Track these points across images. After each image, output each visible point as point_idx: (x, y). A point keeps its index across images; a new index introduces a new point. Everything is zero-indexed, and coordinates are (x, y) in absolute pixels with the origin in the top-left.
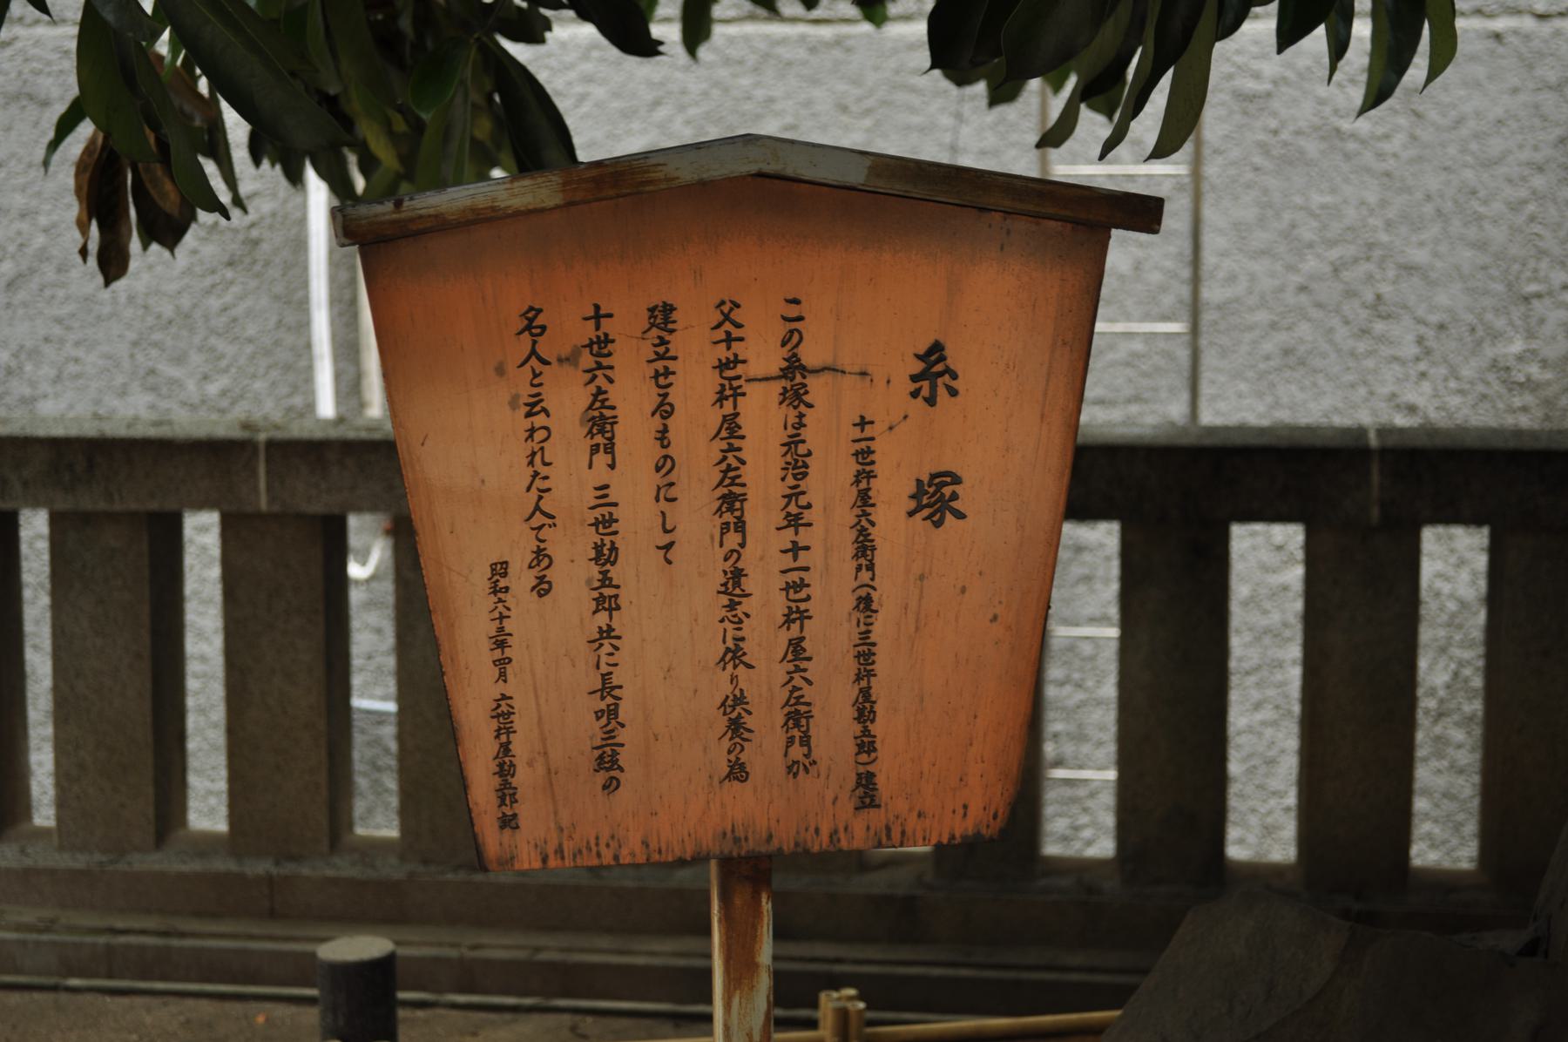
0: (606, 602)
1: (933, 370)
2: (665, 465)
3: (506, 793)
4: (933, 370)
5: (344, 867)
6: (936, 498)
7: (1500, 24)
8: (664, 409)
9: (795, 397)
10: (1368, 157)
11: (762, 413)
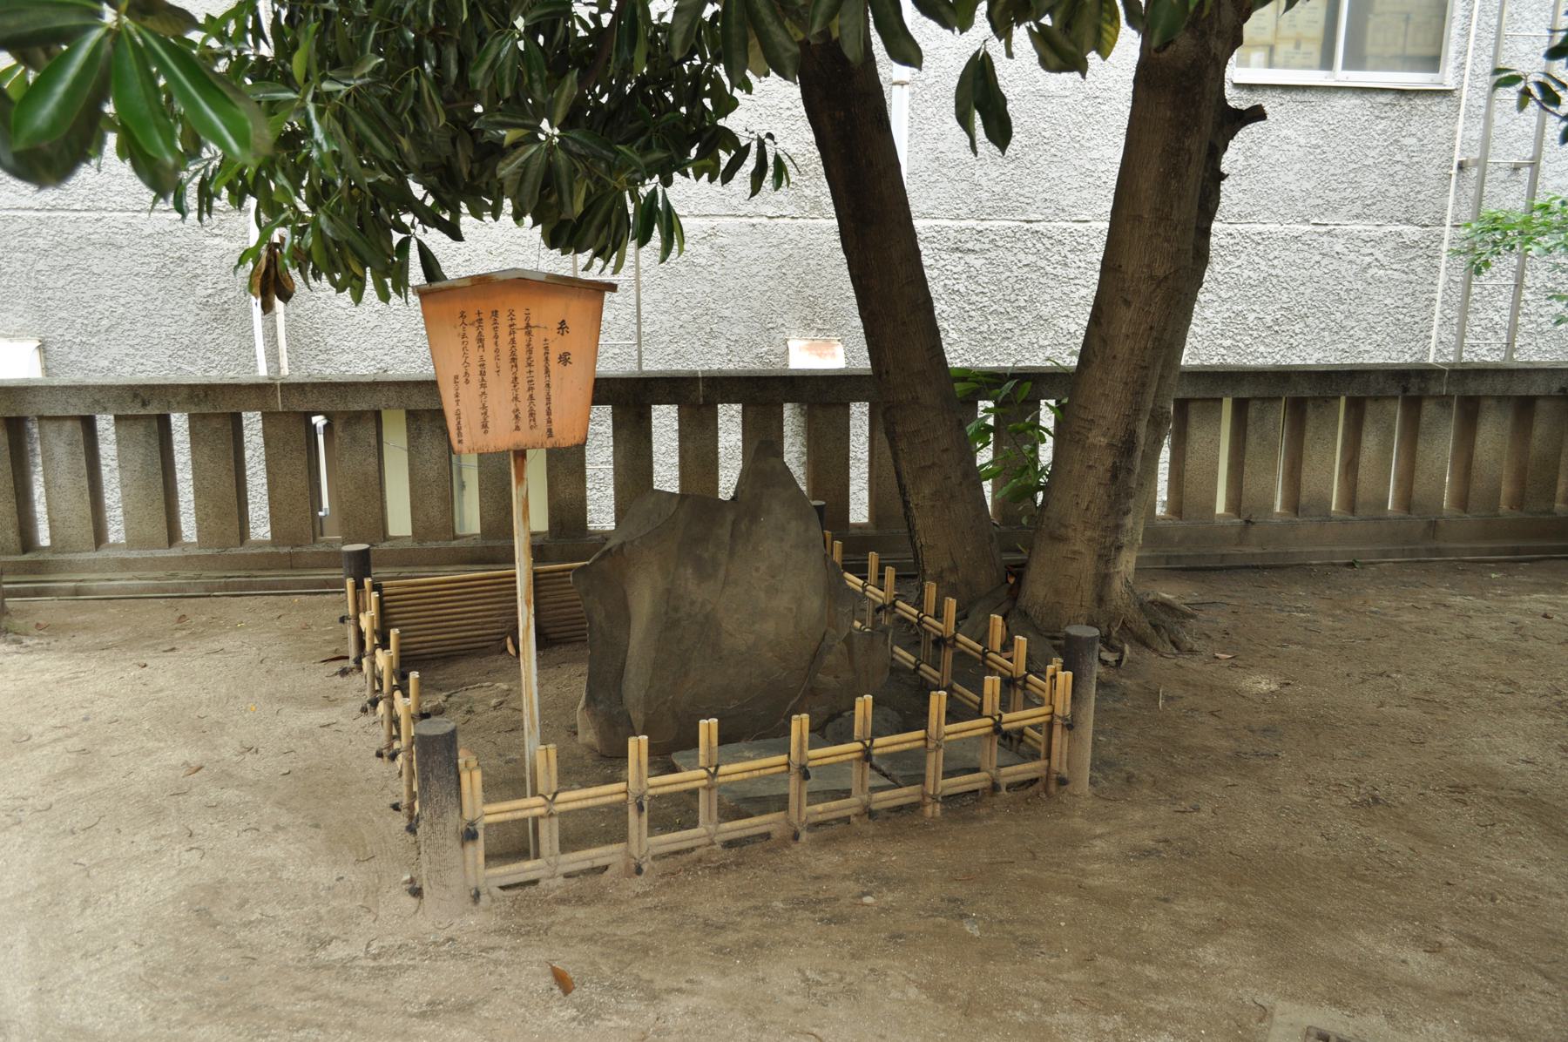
0: (483, 386)
1: (563, 326)
2: (497, 351)
3: (459, 434)
4: (563, 326)
5: (320, 548)
6: (564, 359)
7: (754, 221)
8: (496, 337)
9: (529, 333)
10: (705, 274)
11: (520, 337)
